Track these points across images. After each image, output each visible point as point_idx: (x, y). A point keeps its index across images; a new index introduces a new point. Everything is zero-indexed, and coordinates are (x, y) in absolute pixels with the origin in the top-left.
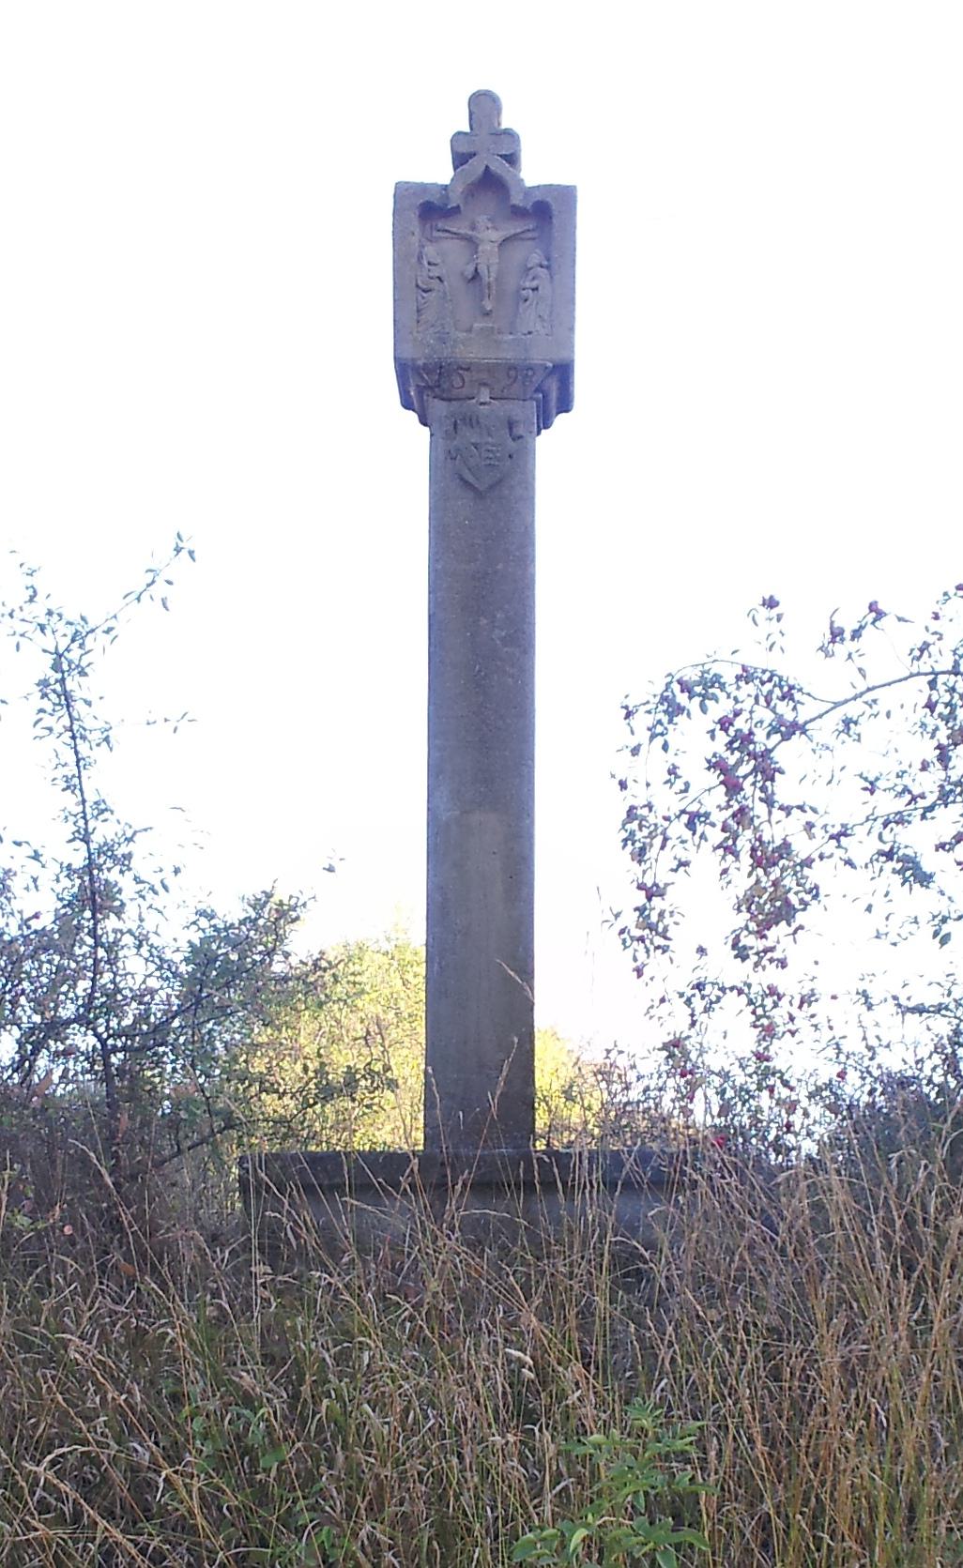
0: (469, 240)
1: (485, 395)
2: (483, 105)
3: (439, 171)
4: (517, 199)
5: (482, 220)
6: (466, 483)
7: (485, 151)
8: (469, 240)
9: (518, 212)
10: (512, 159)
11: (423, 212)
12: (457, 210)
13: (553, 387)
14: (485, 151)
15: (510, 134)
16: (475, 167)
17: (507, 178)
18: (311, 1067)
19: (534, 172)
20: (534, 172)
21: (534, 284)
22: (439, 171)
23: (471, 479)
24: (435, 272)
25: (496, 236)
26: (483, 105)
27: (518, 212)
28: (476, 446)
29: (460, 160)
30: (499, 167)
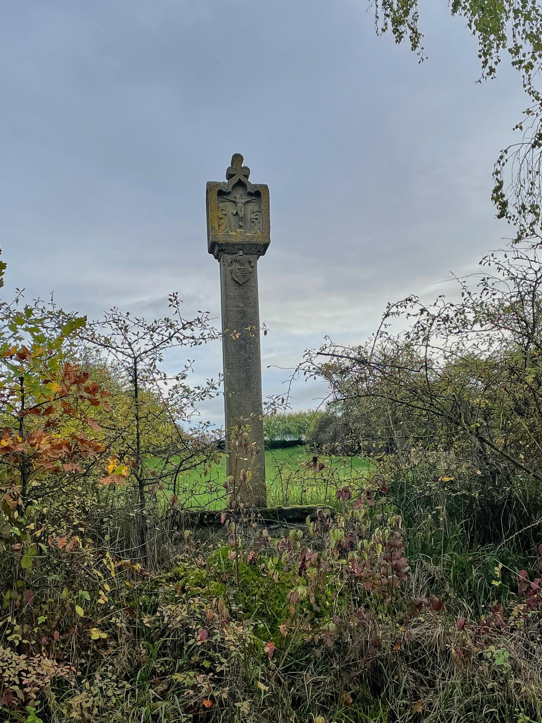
0: (234, 202)
1: (241, 253)
2: (237, 158)
3: (222, 179)
4: (249, 190)
5: (238, 196)
6: (237, 282)
7: (238, 171)
8: (234, 202)
9: (250, 194)
10: (247, 176)
11: (217, 194)
12: (230, 193)
13: (262, 250)
14: (238, 171)
15: (247, 168)
16: (235, 180)
17: (246, 182)
18: (436, 364)
19: (253, 180)
20: (253, 180)
21: (256, 217)
22: (222, 179)
23: (236, 279)
24: (224, 213)
25: (243, 201)
26: (237, 158)
27: (250, 194)
28: (239, 269)
29: (230, 176)
30: (243, 179)
